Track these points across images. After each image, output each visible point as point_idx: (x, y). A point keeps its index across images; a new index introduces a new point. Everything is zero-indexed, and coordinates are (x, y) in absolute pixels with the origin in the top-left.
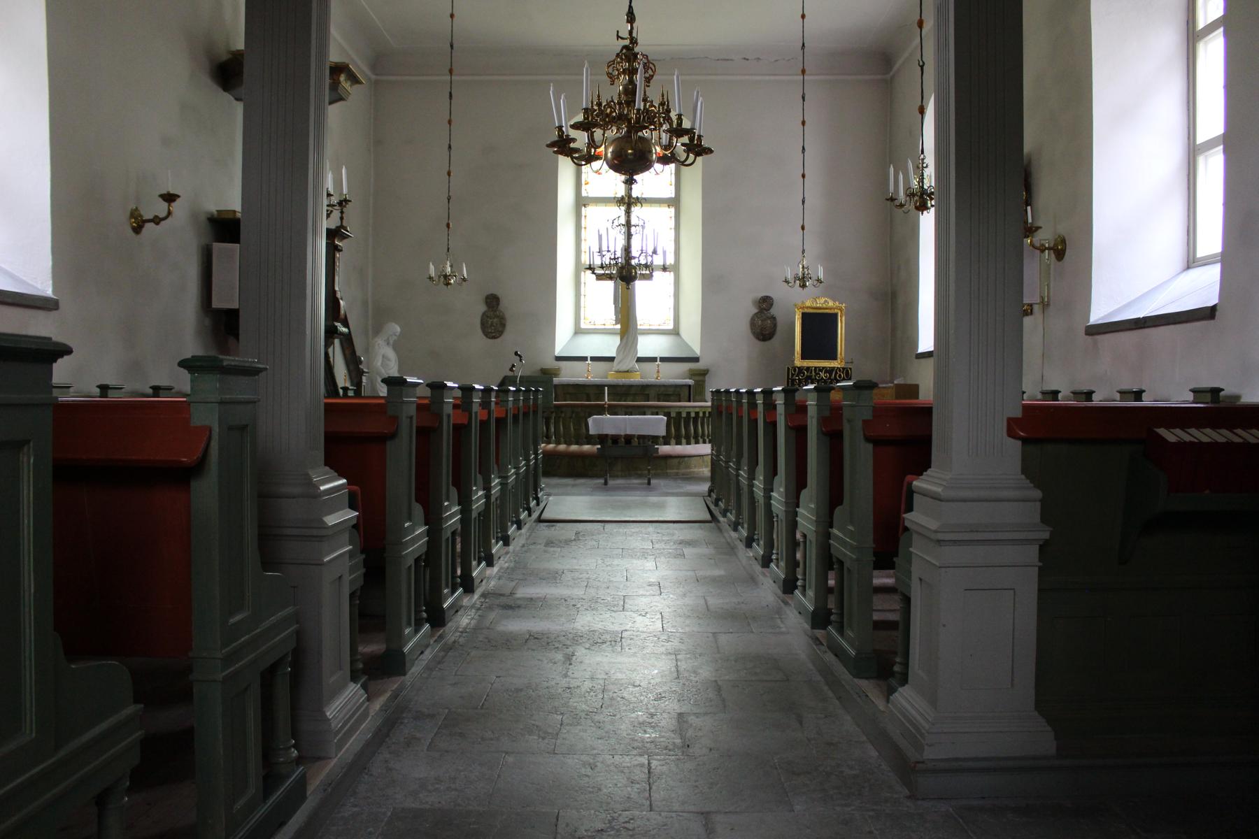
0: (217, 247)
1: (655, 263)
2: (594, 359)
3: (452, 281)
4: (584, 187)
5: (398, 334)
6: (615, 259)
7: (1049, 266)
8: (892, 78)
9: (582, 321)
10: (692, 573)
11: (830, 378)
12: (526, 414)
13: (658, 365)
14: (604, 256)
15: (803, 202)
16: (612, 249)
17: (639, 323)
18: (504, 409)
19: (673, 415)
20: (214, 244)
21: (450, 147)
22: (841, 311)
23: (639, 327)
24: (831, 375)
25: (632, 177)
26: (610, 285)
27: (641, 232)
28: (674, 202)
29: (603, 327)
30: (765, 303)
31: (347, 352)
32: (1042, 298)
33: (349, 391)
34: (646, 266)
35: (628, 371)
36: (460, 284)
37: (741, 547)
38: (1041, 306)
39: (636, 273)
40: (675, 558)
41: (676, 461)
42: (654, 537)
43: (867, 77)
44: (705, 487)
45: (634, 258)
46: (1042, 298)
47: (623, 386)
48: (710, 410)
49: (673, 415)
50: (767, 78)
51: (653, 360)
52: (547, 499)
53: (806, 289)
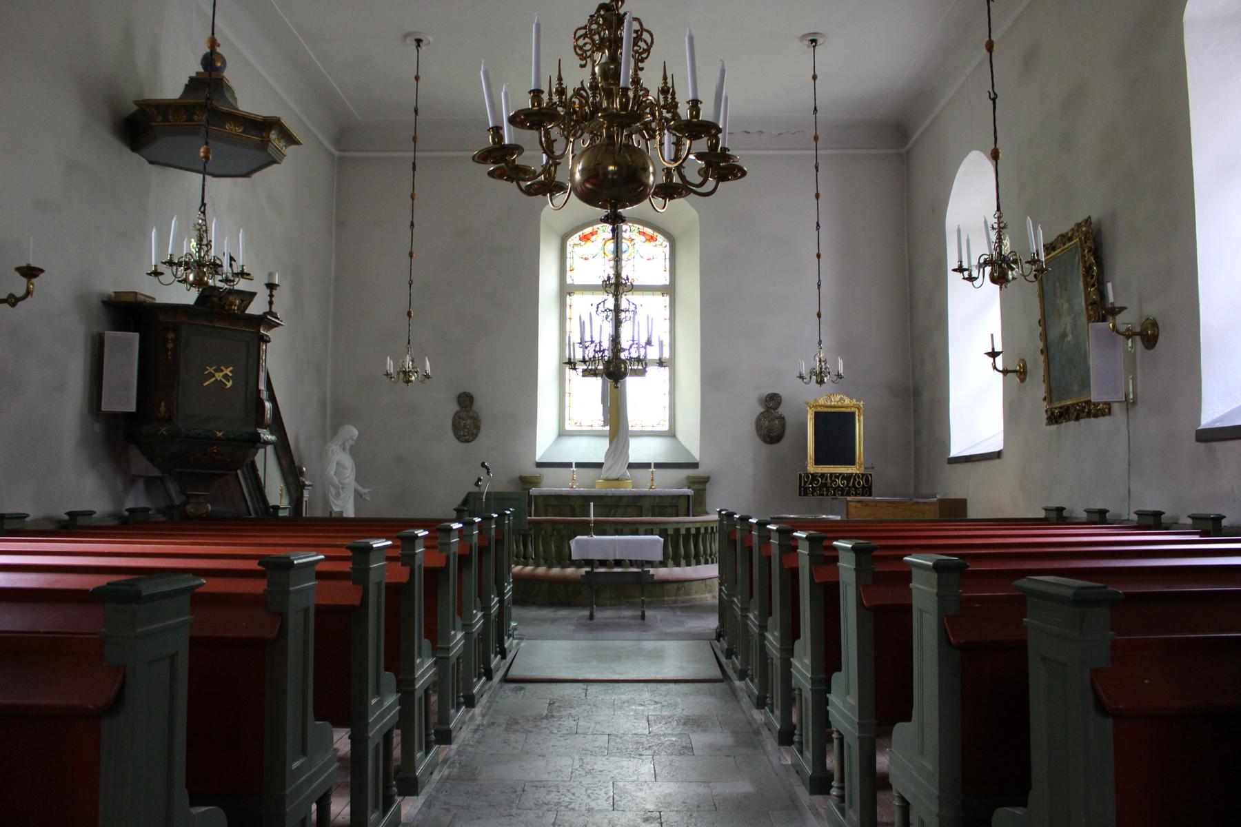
0: (110, 335)
1: (649, 357)
2: (579, 465)
3: (413, 378)
4: (569, 274)
5: (355, 438)
6: (600, 351)
7: (1134, 356)
8: (908, 152)
9: (567, 422)
10: (702, 790)
11: (847, 486)
12: (482, 550)
13: (652, 472)
14: (586, 348)
15: (819, 286)
16: (596, 339)
17: (630, 424)
18: (445, 554)
19: (670, 532)
20: (106, 332)
21: (412, 224)
22: (859, 411)
23: (630, 429)
24: (848, 483)
25: (616, 210)
26: (597, 383)
27: (632, 319)
28: (669, 290)
29: (590, 429)
30: (772, 401)
31: (283, 462)
32: (1127, 396)
33: (280, 511)
34: (638, 360)
35: (617, 480)
36: (422, 382)
37: (771, 743)
38: (1125, 404)
39: (626, 369)
40: (680, 754)
41: (675, 586)
42: (651, 710)
43: (874, 151)
44: (712, 623)
45: (624, 350)
46: (1127, 396)
47: (612, 497)
48: (717, 524)
49: (670, 532)
50: (771, 152)
51: (647, 466)
52: (518, 644)
53: (823, 386)
